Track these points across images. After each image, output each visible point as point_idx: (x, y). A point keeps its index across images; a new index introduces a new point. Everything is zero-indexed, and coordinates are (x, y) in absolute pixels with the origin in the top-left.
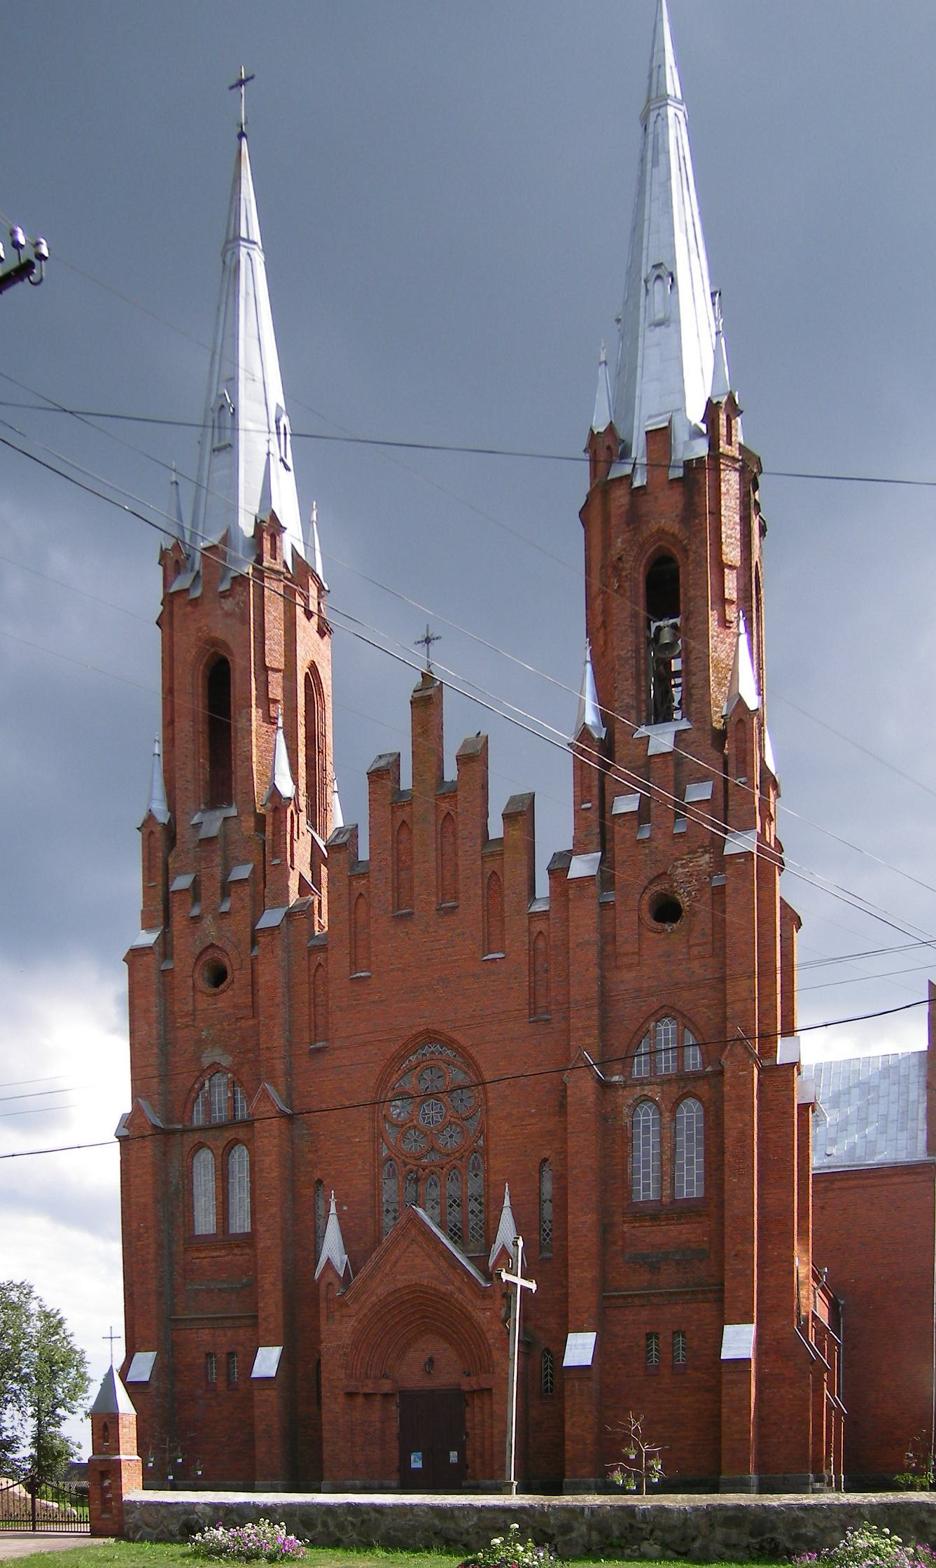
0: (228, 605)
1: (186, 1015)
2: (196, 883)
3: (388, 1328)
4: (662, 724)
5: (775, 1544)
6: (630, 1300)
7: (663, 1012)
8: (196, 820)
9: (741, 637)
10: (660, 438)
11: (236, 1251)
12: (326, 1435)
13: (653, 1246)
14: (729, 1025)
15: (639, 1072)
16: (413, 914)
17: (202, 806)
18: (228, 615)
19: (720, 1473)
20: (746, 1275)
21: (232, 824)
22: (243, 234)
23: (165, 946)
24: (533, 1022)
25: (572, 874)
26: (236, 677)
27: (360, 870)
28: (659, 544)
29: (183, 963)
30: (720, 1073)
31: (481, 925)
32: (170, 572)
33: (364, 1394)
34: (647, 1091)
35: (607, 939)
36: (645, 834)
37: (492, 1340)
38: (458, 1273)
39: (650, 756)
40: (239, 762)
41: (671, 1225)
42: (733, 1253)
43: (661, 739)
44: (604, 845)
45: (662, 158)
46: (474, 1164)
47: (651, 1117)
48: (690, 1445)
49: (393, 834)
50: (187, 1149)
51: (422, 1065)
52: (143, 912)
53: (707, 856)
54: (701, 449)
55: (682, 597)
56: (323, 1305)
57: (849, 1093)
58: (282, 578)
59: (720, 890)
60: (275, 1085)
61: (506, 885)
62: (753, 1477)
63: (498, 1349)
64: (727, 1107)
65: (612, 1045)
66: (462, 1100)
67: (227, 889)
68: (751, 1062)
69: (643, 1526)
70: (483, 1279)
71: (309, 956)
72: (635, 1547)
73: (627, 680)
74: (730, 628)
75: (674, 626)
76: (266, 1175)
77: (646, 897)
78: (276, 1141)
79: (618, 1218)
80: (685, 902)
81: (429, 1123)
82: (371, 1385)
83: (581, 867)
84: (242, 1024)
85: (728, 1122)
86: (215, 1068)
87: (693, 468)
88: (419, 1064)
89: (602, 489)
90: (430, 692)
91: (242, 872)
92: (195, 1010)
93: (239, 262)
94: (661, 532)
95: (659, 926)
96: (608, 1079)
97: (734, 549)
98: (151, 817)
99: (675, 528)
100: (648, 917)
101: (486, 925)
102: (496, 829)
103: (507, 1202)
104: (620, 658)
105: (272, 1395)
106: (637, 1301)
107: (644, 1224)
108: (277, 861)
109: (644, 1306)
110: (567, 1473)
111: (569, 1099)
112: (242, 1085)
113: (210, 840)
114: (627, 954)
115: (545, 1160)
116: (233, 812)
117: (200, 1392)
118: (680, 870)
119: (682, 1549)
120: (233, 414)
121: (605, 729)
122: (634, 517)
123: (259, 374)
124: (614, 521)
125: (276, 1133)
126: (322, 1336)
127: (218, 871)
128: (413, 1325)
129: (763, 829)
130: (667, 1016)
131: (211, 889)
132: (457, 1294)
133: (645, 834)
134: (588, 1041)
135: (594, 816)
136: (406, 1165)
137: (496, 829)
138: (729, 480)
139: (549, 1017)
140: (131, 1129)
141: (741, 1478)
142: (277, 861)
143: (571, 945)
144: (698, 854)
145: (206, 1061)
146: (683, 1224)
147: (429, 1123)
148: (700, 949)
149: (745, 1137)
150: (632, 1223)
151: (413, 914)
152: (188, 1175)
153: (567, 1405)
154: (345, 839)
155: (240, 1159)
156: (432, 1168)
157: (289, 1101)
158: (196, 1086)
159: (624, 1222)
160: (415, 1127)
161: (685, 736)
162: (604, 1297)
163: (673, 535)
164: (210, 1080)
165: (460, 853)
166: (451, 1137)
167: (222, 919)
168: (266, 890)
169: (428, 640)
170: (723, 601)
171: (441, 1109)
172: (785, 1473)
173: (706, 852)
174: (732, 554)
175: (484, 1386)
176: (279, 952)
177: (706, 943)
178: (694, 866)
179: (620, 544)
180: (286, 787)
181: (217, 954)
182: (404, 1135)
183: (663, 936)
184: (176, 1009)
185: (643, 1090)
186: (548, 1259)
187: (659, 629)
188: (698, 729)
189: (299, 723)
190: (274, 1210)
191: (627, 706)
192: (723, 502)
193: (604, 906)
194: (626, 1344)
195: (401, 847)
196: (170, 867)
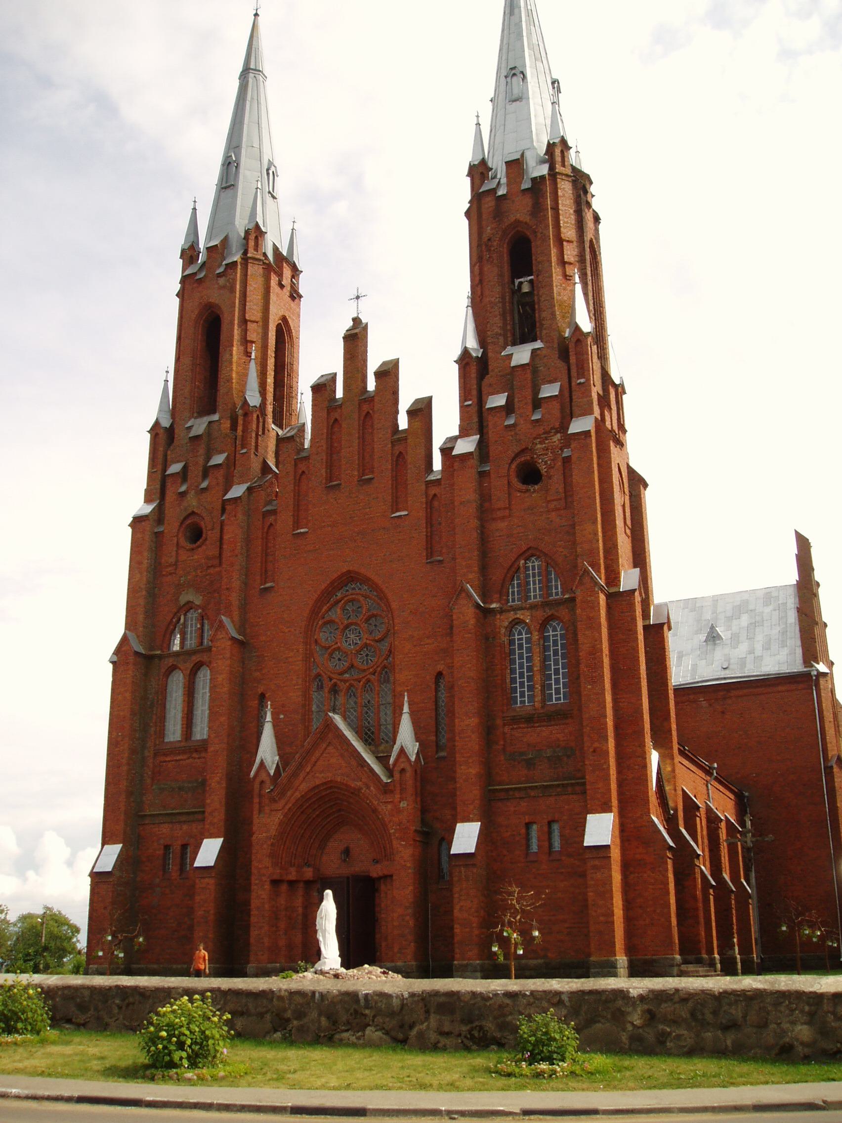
0: (222, 281)
1: (170, 566)
2: (185, 468)
3: (310, 820)
4: (521, 346)
5: (483, 1033)
6: (511, 793)
7: (530, 552)
8: (189, 424)
9: (577, 285)
10: (515, 166)
11: (195, 755)
12: (253, 919)
13: (529, 745)
14: (579, 561)
16: (340, 484)
17: (195, 415)
18: (224, 287)
19: (589, 955)
20: (604, 769)
21: (215, 426)
22: (252, 66)
23: (159, 515)
24: (430, 562)
25: (455, 452)
26: (225, 327)
27: (304, 454)
28: (516, 229)
29: (171, 526)
30: (573, 600)
31: (390, 491)
32: (477, 181)
34: (520, 615)
35: (484, 497)
36: (511, 421)
37: (393, 831)
38: (365, 771)
39: (514, 367)
40: (222, 384)
41: (543, 726)
42: (591, 750)
43: (521, 355)
44: (482, 430)
45: (516, 11)
46: (384, 678)
48: (567, 928)
49: (328, 428)
50: (163, 670)
51: (346, 599)
52: (146, 490)
53: (559, 436)
54: (544, 170)
55: (534, 262)
56: (256, 800)
58: (261, 263)
60: (230, 616)
61: (409, 461)
62: (622, 960)
63: (397, 838)
64: (580, 626)
65: (491, 579)
66: (375, 626)
67: (206, 472)
68: (596, 589)
69: (367, 1012)
70: (385, 776)
71: (264, 518)
72: (360, 1034)
73: (496, 317)
74: (570, 280)
75: (531, 282)
77: (513, 466)
78: (228, 662)
79: (499, 722)
80: (543, 469)
81: (350, 644)
82: (294, 873)
83: (466, 446)
84: (212, 570)
85: (581, 638)
86: (189, 606)
87: (538, 182)
88: (342, 599)
89: (477, 198)
90: (356, 331)
91: (218, 459)
92: (177, 561)
93: (248, 82)
94: (517, 222)
95: (524, 487)
96: (487, 606)
97: (570, 230)
98: (466, 353)
99: (527, 218)
100: (515, 481)
101: (394, 491)
102: (403, 422)
103: (406, 709)
104: (491, 302)
105: (210, 882)
106: (517, 795)
107: (521, 726)
108: (244, 451)
109: (523, 798)
110: (457, 956)
111: (455, 622)
112: (208, 619)
113: (197, 437)
114: (499, 509)
115: (440, 675)
116: (216, 417)
117: (157, 881)
118: (539, 446)
119: (401, 1036)
120: (236, 167)
121: (482, 350)
122: (498, 213)
123: (256, 145)
124: (484, 217)
125: (228, 655)
127: (201, 460)
128: (332, 818)
129: (602, 415)
130: (532, 555)
131: (195, 472)
132: (364, 789)
133: (511, 421)
134: (471, 576)
135: (475, 409)
136: (331, 679)
137: (403, 422)
138: (564, 188)
139: (442, 559)
140: (119, 656)
141: (608, 960)
142: (244, 451)
143: (456, 503)
144: (552, 434)
145: (183, 599)
146: (553, 725)
147: (350, 644)
148: (555, 503)
149: (595, 651)
151: (340, 484)
152: (163, 693)
154: (292, 433)
155: (204, 677)
156: (352, 682)
157: (241, 629)
158: (174, 620)
159: (504, 725)
160: (338, 649)
161: (539, 352)
162: (490, 790)
163: (526, 223)
164: (185, 615)
165: (376, 440)
166: (367, 655)
167: (202, 493)
168: (236, 471)
169: (358, 298)
170: (563, 263)
171: (360, 633)
172: (653, 955)
173: (557, 432)
174: (569, 231)
175: (386, 873)
176: (240, 517)
177: (560, 499)
178: (549, 443)
179: (489, 231)
180: (254, 399)
181: (196, 519)
182: (331, 654)
183: (527, 495)
184: (163, 560)
185: (516, 614)
186: (444, 758)
187: (521, 283)
188: (548, 348)
189: (269, 356)
190: (223, 719)
191: (497, 334)
192: (560, 202)
193: (482, 474)
195: (334, 437)
196: (169, 457)
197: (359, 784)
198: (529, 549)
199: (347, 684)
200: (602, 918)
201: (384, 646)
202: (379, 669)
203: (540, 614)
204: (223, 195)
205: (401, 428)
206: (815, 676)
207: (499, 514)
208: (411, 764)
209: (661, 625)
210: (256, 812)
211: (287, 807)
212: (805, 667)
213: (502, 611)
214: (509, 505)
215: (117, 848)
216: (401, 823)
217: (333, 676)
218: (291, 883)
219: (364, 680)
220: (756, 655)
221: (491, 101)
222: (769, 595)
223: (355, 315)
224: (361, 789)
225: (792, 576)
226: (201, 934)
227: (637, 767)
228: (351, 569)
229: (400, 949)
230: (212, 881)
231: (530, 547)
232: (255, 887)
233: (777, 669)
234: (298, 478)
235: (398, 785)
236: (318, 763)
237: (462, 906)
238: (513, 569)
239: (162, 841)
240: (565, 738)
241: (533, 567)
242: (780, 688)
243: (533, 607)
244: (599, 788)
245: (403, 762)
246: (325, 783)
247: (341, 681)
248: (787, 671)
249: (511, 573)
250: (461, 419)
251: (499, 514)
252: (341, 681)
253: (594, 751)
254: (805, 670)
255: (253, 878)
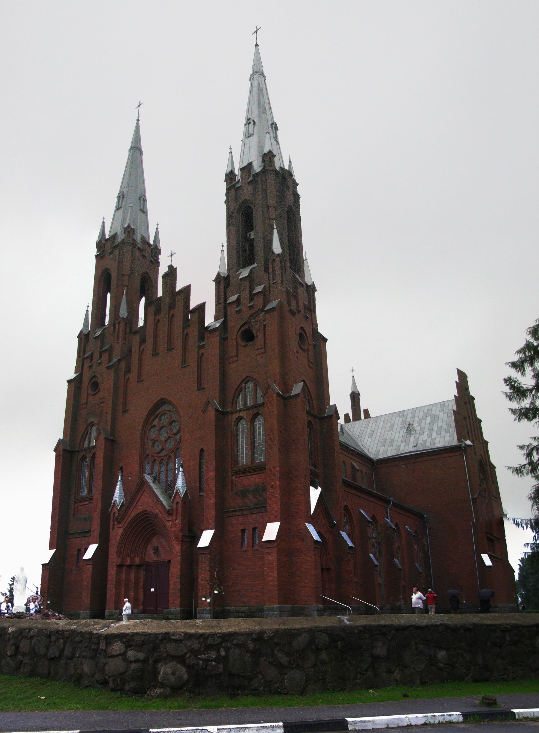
6: (234, 513)
7: (248, 378)
15: (239, 407)
33: (126, 565)
34: (241, 414)
47: (244, 426)
48: (261, 588)
50: (79, 459)
51: (161, 414)
52: (76, 367)
57: (426, 419)
59: (265, 325)
76: (98, 466)
77: (240, 333)
105: (89, 568)
114: (232, 357)
126: (110, 538)
130: (249, 381)
150: (236, 475)
153: (200, 567)
156: (163, 457)
159: (232, 475)
167: (99, 365)
171: (167, 431)
172: (305, 604)
185: (239, 414)
194: (233, 535)
197: (157, 511)
198: (247, 377)
199: (161, 459)
200: (271, 583)
201: (178, 437)
202: (175, 449)
203: (251, 412)
204: (117, 212)
205: (207, 324)
206: (464, 447)
207: (232, 360)
208: (181, 499)
209: (331, 417)
210: (111, 529)
211: (125, 526)
212: (459, 443)
213: (232, 413)
214: (237, 354)
215: (54, 551)
216: (176, 531)
217: (154, 455)
218: (129, 566)
219: (168, 456)
220: (432, 438)
221: (242, 141)
222: (443, 405)
223: (170, 264)
224: (158, 514)
225: (452, 392)
226: (85, 595)
227: (298, 495)
228: (162, 397)
229: (173, 601)
230: (91, 567)
231: (247, 376)
232: (110, 569)
233: (443, 445)
234: (141, 352)
235: (175, 511)
236: (139, 501)
237: (202, 577)
238: (239, 389)
239: (76, 547)
240: (263, 481)
241: (249, 387)
242: (445, 455)
243: (249, 409)
244: (274, 508)
245: (177, 498)
246: (143, 512)
247: (158, 457)
248: (448, 445)
249: (238, 391)
250: (216, 312)
251: (232, 360)
252: (158, 457)
253: (272, 487)
254: (458, 444)
255: (109, 564)
